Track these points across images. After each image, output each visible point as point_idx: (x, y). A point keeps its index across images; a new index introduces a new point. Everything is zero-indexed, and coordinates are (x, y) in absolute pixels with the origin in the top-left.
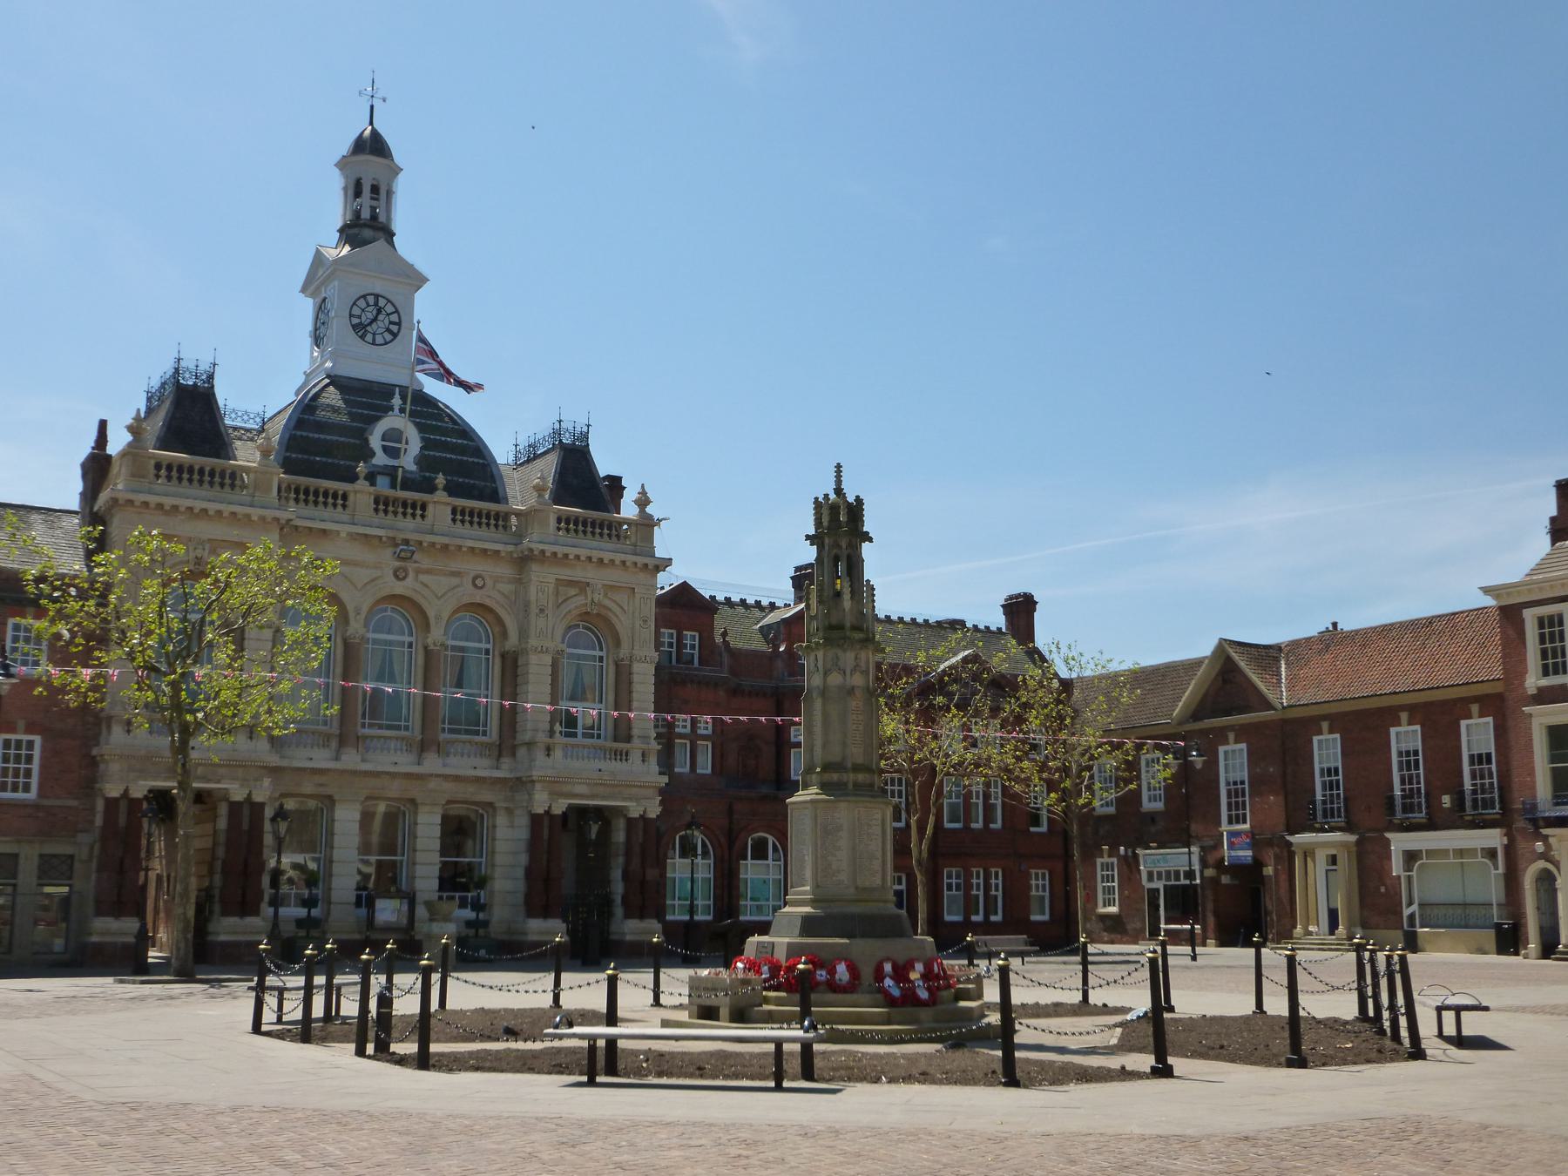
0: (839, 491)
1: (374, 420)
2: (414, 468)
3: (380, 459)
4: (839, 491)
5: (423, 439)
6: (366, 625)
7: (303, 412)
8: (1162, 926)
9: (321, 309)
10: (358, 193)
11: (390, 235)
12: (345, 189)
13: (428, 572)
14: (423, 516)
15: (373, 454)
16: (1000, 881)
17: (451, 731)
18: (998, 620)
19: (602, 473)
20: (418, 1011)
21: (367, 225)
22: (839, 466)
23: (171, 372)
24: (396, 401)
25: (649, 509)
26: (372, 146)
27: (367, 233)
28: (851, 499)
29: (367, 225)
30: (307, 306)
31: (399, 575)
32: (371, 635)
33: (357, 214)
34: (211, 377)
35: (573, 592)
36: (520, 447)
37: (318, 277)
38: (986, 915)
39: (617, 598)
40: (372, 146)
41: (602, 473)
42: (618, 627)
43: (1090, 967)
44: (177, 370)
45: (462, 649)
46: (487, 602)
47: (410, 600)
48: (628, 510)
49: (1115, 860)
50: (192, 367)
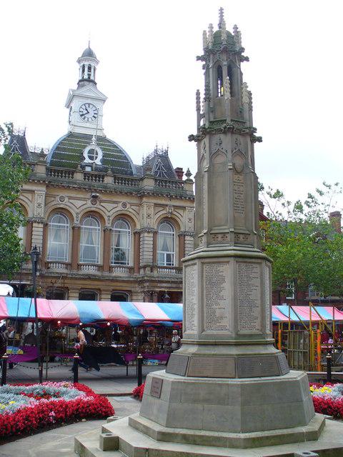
0: (222, 24)
1: (85, 147)
2: (100, 164)
3: (87, 160)
7: (59, 144)
13: (105, 201)
14: (103, 181)
20: (142, 367)
21: (87, 80)
22: (221, 10)
26: (89, 54)
27: (86, 83)
28: (229, 28)
29: (87, 80)
40: (89, 54)
46: (128, 213)
50: (33, 146)
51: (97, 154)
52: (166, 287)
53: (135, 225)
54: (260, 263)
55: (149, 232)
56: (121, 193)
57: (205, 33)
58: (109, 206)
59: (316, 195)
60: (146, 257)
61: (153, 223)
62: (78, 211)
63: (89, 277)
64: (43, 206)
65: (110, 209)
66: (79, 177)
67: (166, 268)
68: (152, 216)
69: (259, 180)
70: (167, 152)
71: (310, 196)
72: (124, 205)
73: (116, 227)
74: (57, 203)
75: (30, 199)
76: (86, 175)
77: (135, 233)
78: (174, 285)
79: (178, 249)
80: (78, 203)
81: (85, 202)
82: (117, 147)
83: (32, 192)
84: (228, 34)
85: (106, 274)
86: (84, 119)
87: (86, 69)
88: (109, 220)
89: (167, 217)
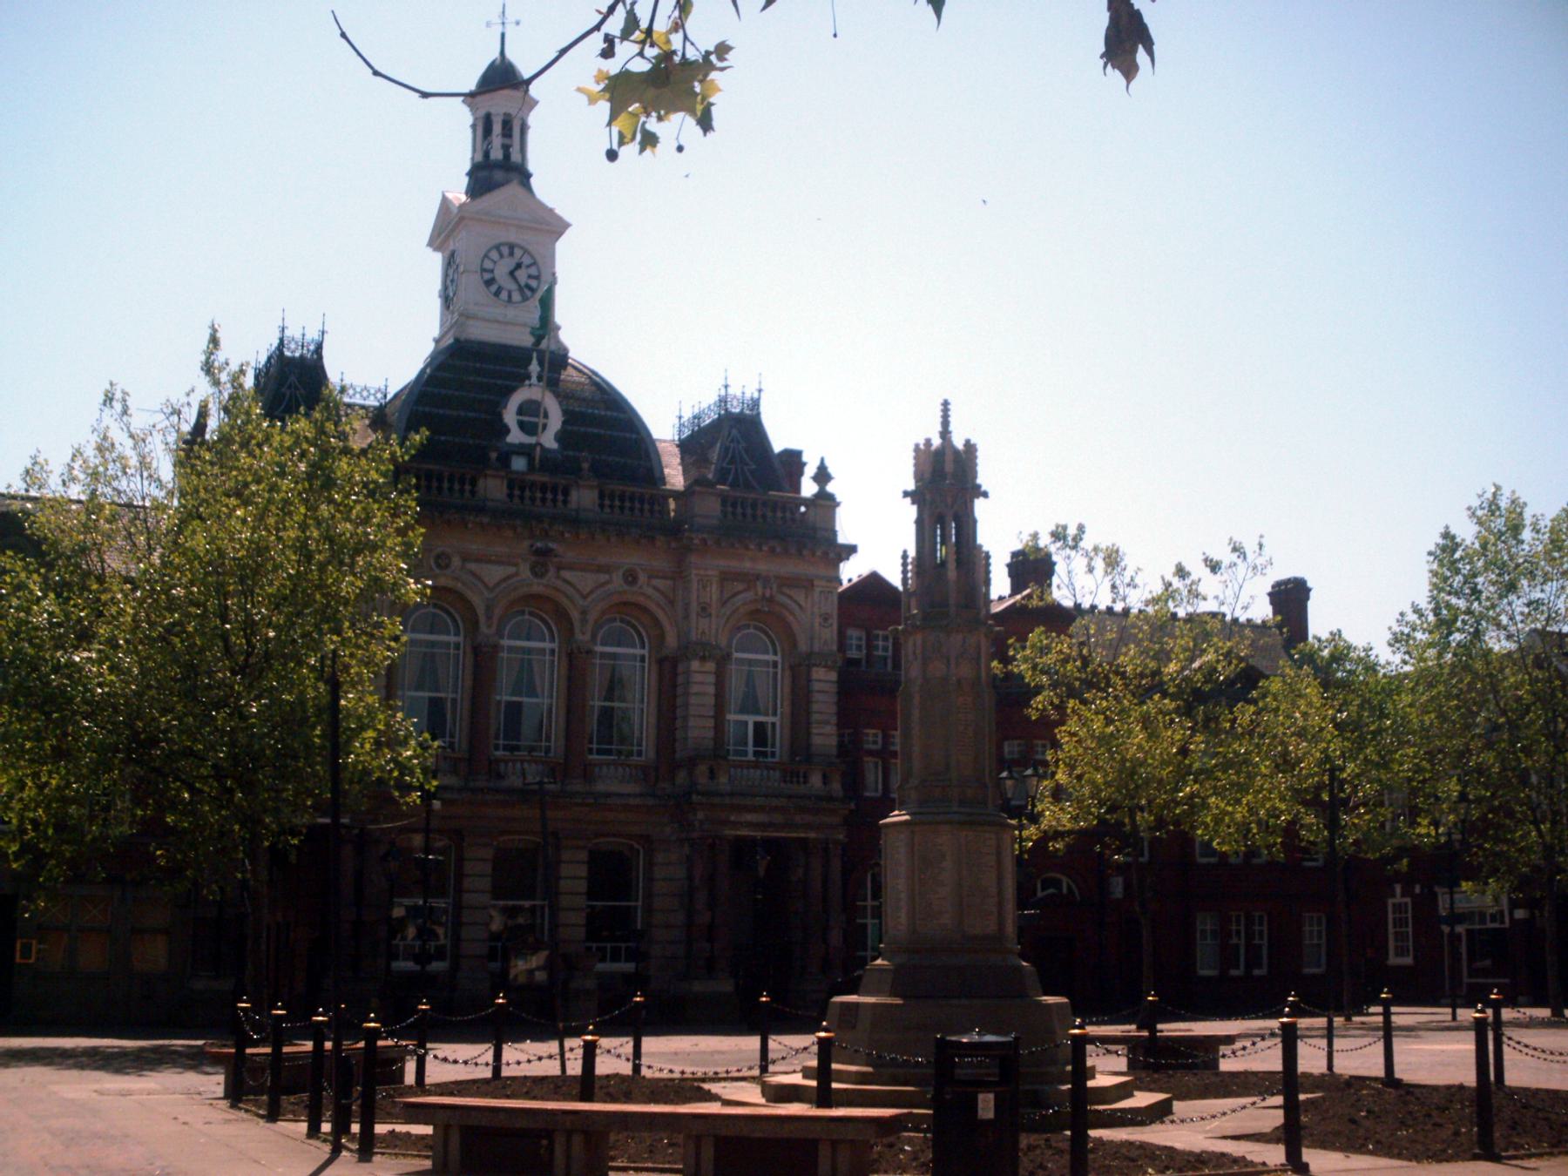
0: (945, 433)
1: (510, 391)
2: (554, 445)
3: (516, 436)
4: (945, 433)
5: (565, 412)
6: (594, 636)
8: (1466, 980)
9: (450, 263)
10: (488, 131)
11: (524, 176)
12: (474, 126)
13: (571, 567)
14: (565, 502)
15: (507, 431)
16: (1265, 928)
17: (599, 752)
18: (1262, 611)
19: (778, 446)
23: (276, 343)
24: (534, 368)
25: (830, 488)
27: (499, 175)
28: (959, 443)
30: (436, 260)
31: (538, 571)
32: (599, 649)
33: (487, 154)
34: (319, 347)
35: (740, 587)
36: (684, 419)
37: (448, 229)
38: (1249, 966)
39: (791, 593)
41: (778, 446)
42: (795, 627)
43: (1507, 1032)
44: (281, 340)
45: (614, 656)
46: (641, 599)
47: (548, 599)
48: (808, 488)
49: (1408, 900)
51: (546, 416)
52: (750, 825)
55: (703, 659)
57: (917, 446)
58: (585, 581)
59: (1198, 570)
60: (698, 729)
66: (493, 488)
67: (756, 765)
70: (756, 403)
71: (1181, 572)
72: (631, 577)
73: (603, 644)
76: (516, 484)
77: (661, 662)
78: (778, 818)
79: (787, 709)
80: (494, 573)
81: (512, 570)
84: (956, 452)
86: (497, 294)
87: (497, 128)
88: (584, 621)
89: (757, 611)
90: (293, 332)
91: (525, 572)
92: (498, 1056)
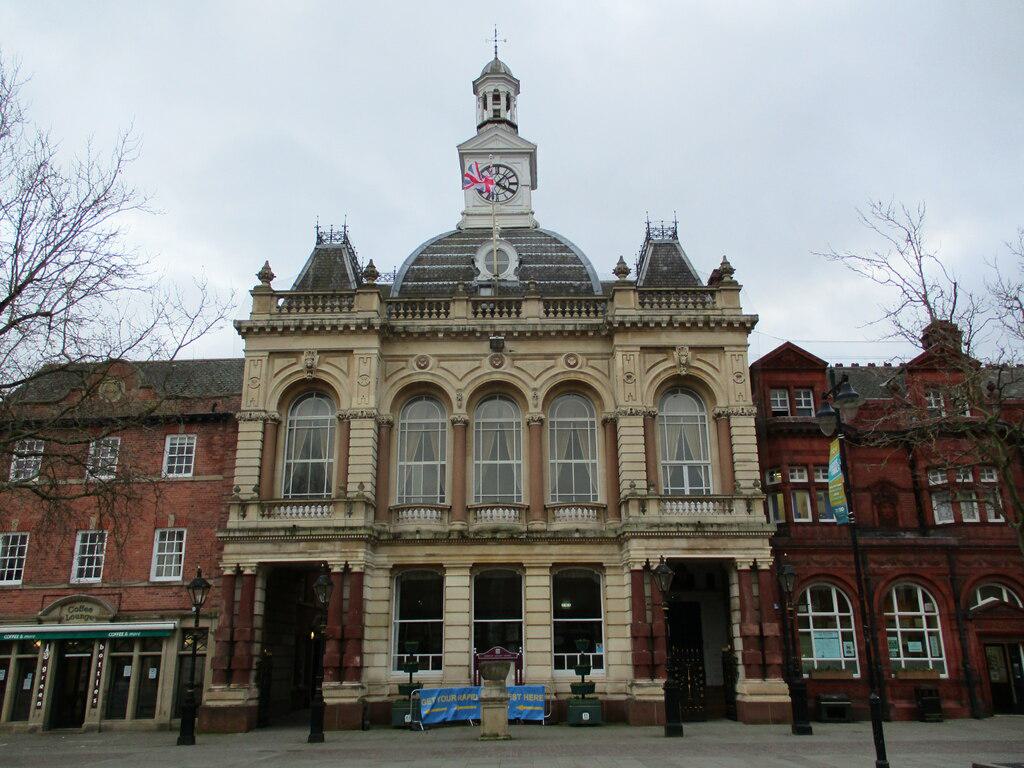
2: (515, 278)
13: (524, 357)
31: (497, 364)
46: (582, 378)
53: (602, 406)
54: (481, 360)
56: (562, 335)
58: (535, 366)
61: (643, 394)
62: (461, 385)
63: (494, 536)
64: (373, 380)
65: (534, 373)
68: (637, 376)
69: (717, 268)
74: (413, 373)
75: (345, 369)
81: (477, 364)
82: (560, 242)
83: (348, 352)
85: (538, 525)
87: (490, 100)
88: (536, 397)
90: (325, 229)
91: (486, 367)
92: (583, 677)
